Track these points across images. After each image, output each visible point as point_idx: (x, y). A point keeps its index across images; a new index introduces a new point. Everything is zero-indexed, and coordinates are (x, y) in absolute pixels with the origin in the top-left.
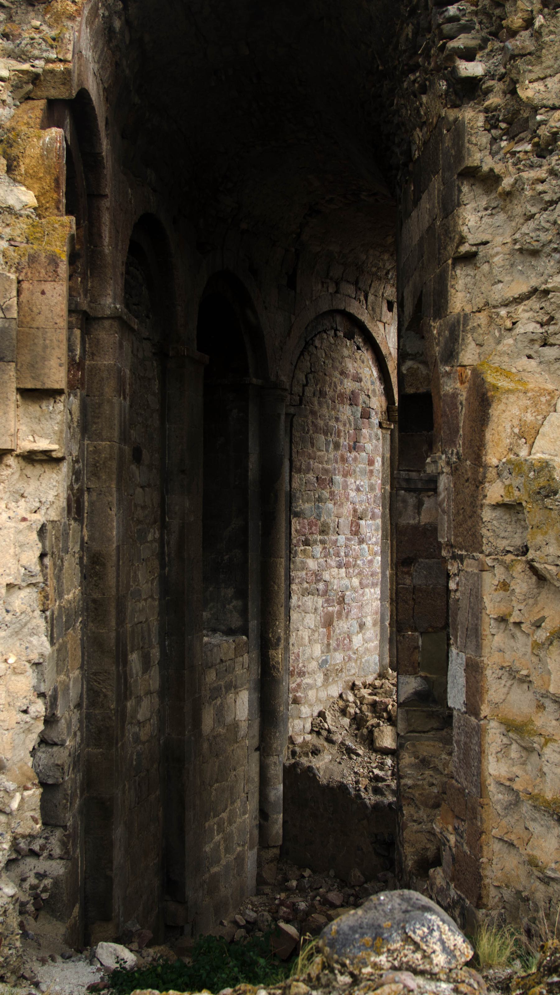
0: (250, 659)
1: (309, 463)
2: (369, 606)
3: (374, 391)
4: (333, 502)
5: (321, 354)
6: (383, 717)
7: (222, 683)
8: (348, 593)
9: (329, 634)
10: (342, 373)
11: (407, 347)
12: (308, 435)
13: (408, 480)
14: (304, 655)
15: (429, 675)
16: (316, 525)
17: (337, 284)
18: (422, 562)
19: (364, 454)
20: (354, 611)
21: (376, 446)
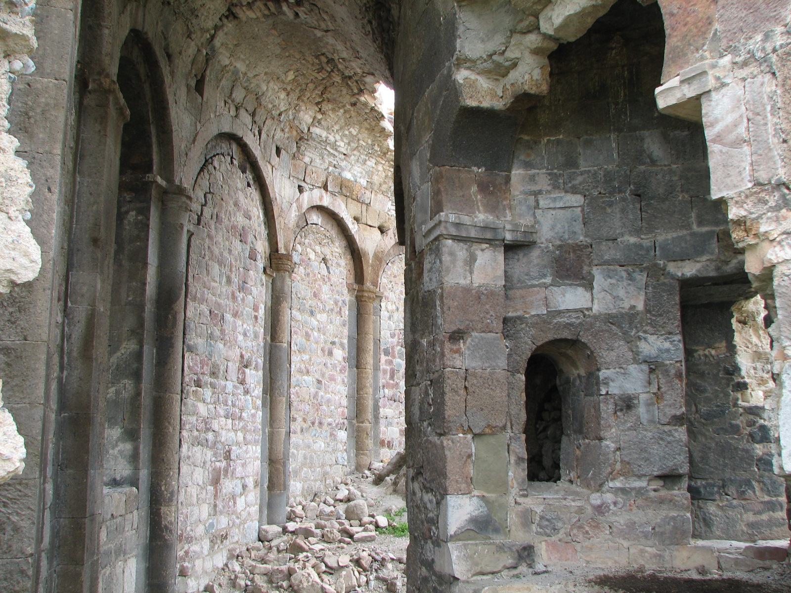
0: (140, 517)
1: (204, 292)
3: (260, 233)
6: (281, 587)
8: (234, 448)
9: (216, 492)
10: (236, 204)
11: (467, 50)
12: (204, 261)
13: (458, 225)
16: (207, 365)
17: (237, 109)
19: (250, 297)
21: (261, 292)
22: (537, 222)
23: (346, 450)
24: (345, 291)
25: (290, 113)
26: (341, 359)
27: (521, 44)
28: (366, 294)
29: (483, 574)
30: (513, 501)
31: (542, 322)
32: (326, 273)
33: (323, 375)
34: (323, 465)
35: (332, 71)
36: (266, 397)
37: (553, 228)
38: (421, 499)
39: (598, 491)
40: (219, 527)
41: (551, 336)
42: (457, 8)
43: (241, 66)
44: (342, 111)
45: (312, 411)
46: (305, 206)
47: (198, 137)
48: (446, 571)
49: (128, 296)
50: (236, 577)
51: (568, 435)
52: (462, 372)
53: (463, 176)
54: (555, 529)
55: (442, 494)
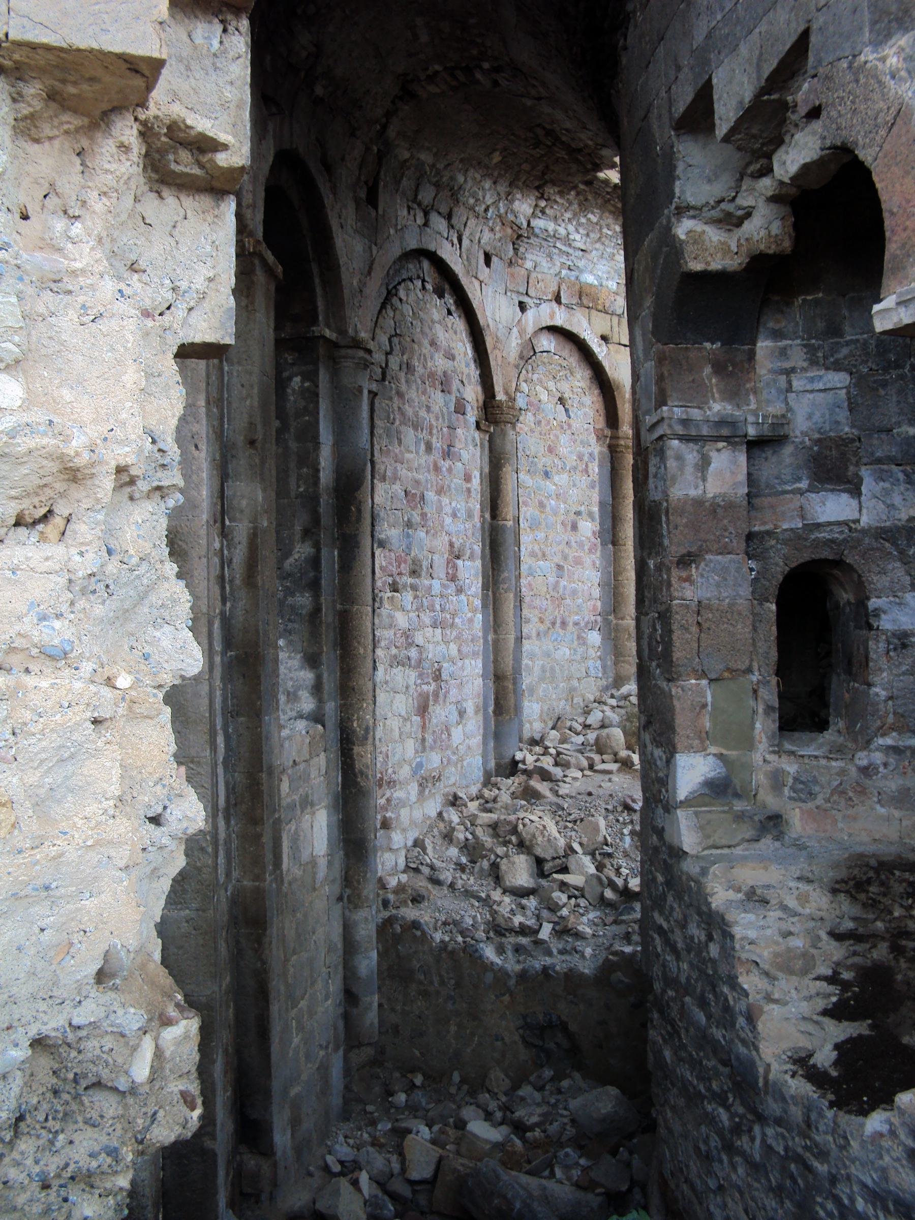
2: (470, 685)
3: (469, 375)
4: (425, 529)
5: (407, 310)
6: (510, 842)
7: (296, 797)
8: (445, 665)
9: (424, 723)
10: (433, 343)
11: (688, 194)
13: (685, 422)
14: (394, 755)
15: (725, 752)
16: (405, 562)
17: (426, 214)
18: (711, 561)
19: (459, 464)
20: (454, 692)
21: (474, 455)
22: (789, 409)
23: (600, 658)
24: (593, 439)
25: (501, 205)
26: (590, 534)
27: (754, 189)
28: (622, 442)
29: (717, 848)
30: (761, 759)
31: (796, 538)
32: (565, 418)
33: (565, 558)
34: (569, 678)
35: (554, 144)
36: (487, 595)
37: (810, 417)
38: (652, 754)
39: (865, 749)
40: (429, 767)
41: (806, 556)
42: (674, 138)
43: (426, 157)
44: (573, 193)
45: (551, 608)
46: (530, 330)
47: (376, 266)
48: (675, 842)
49: (299, 487)
50: (453, 829)
51: (838, 675)
52: (694, 605)
53: (692, 355)
54: (811, 794)
55: (671, 752)
